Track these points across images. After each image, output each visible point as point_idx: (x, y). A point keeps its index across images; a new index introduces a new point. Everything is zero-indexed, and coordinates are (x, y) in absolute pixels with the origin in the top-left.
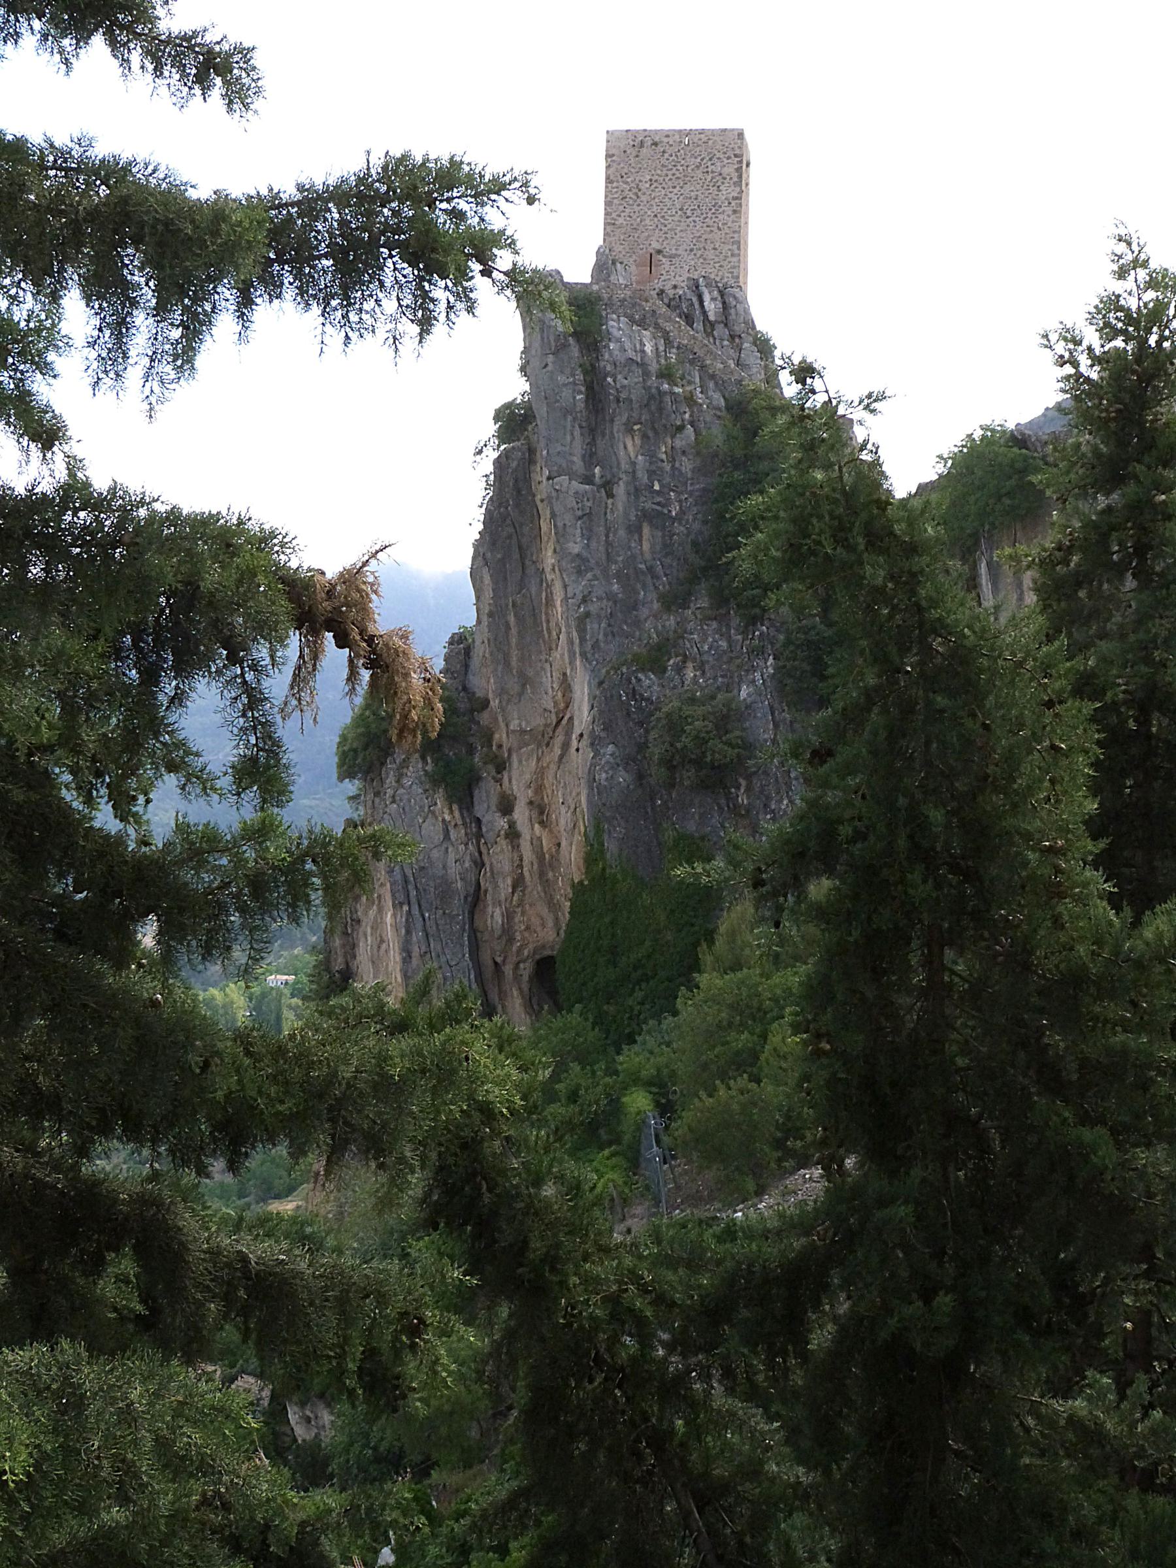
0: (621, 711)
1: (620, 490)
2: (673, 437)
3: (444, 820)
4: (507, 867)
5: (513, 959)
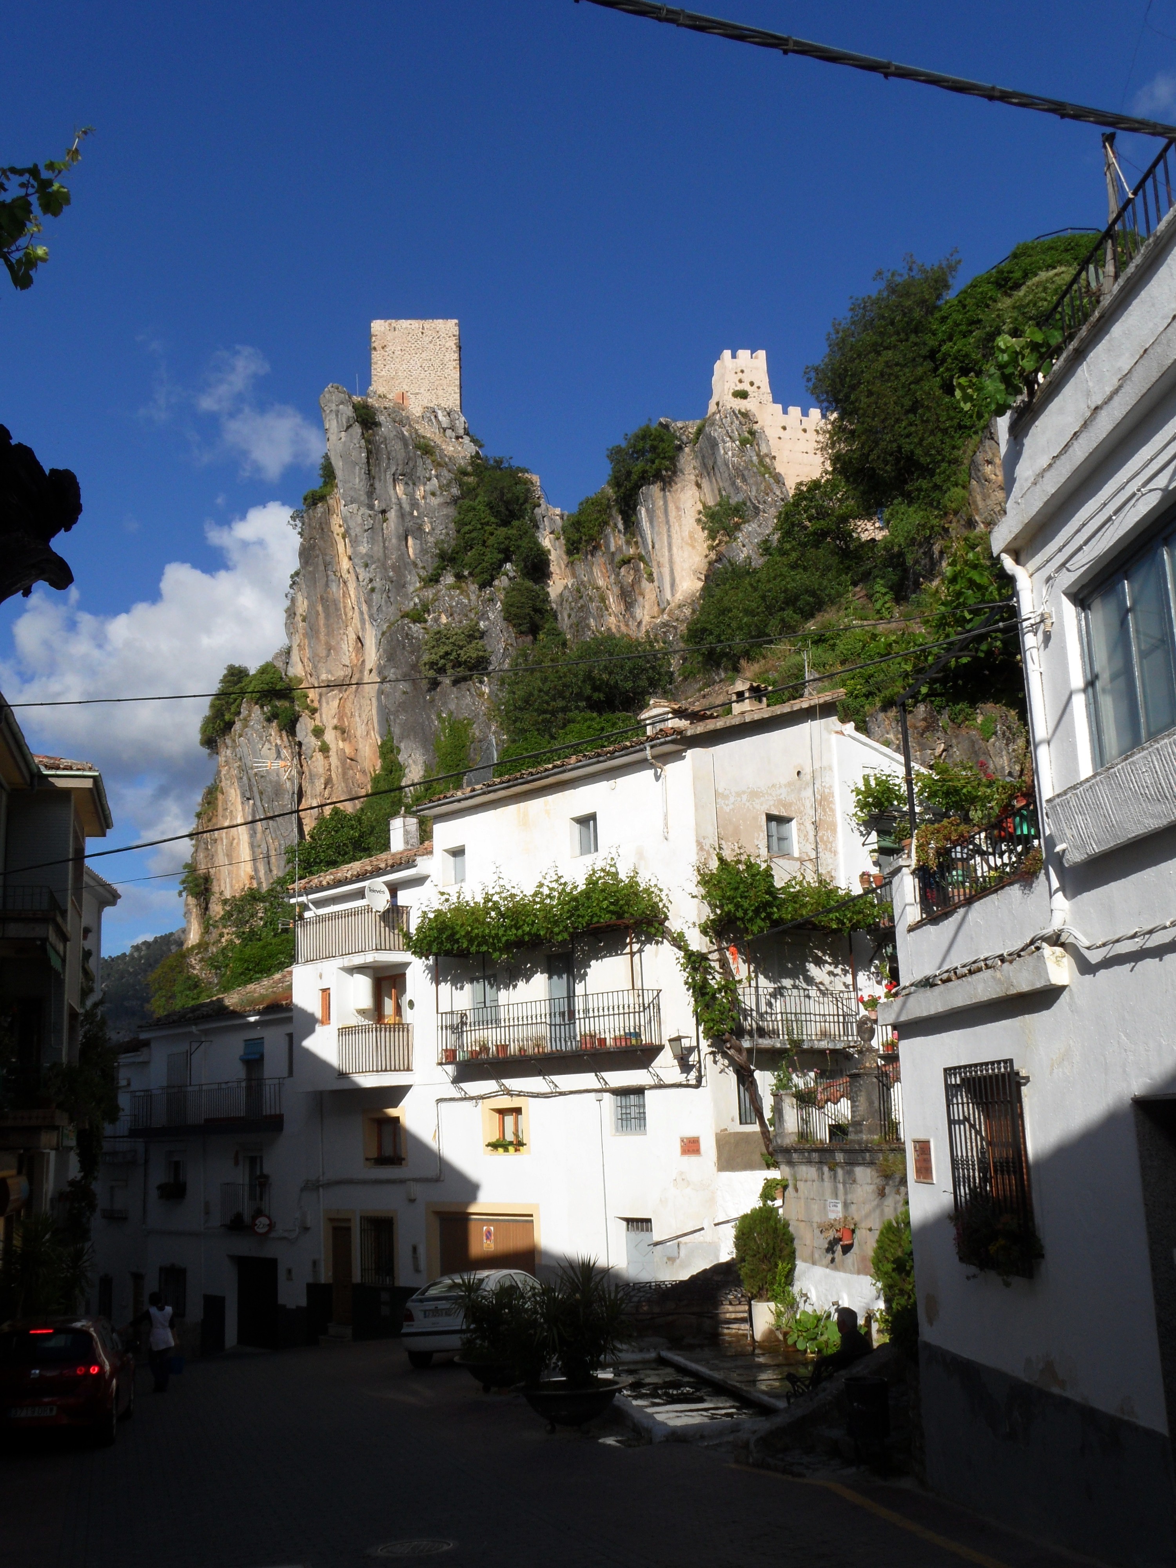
0: (394, 646)
1: (392, 515)
2: (425, 484)
3: (276, 745)
4: (321, 770)
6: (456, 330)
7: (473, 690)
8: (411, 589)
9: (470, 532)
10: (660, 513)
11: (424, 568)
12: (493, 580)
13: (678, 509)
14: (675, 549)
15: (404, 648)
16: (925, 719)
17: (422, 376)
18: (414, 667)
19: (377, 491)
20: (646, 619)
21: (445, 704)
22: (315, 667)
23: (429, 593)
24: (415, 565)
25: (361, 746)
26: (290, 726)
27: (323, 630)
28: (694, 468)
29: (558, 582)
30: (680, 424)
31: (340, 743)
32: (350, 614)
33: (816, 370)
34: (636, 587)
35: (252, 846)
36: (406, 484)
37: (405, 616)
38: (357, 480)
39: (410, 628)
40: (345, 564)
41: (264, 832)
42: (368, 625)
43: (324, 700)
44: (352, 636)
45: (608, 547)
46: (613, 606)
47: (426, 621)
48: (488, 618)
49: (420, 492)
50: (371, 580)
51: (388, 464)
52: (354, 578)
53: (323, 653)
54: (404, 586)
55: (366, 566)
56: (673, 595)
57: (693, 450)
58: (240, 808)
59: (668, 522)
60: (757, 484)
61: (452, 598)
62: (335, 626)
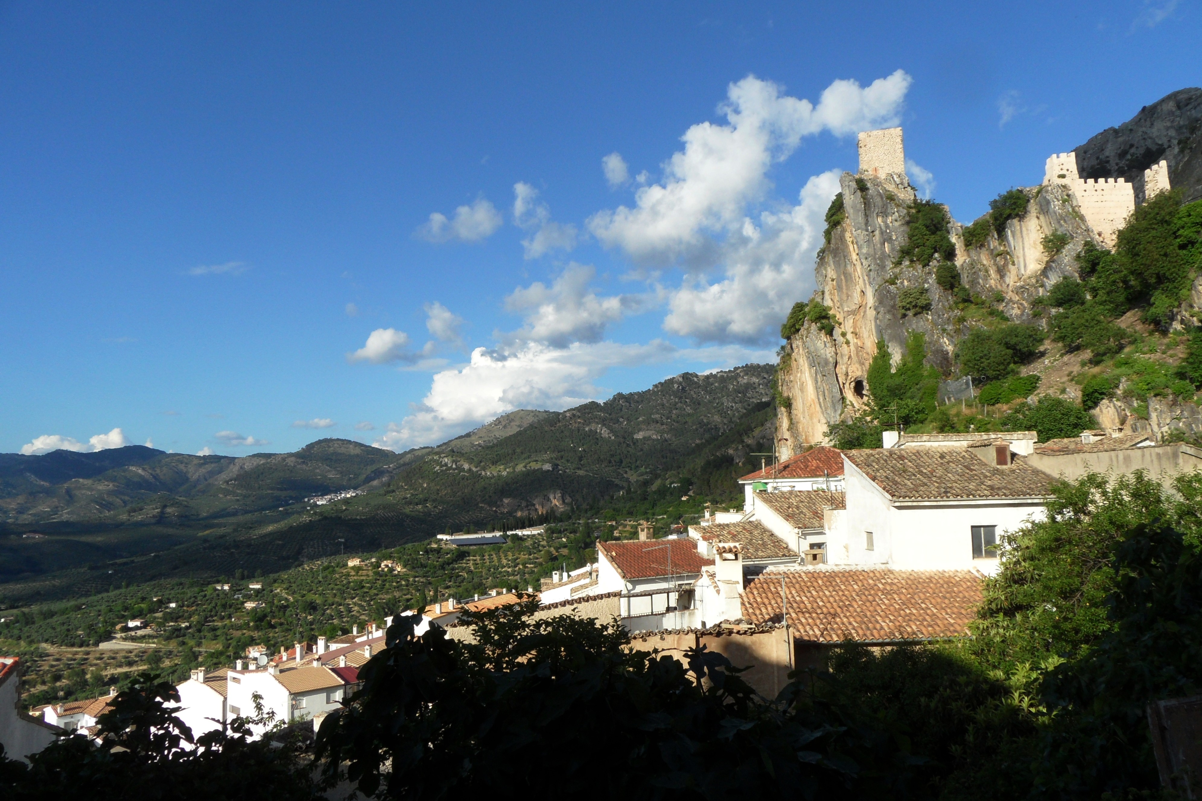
0: (882, 297)
1: (877, 233)
5: (848, 382)
6: (901, 133)
13: (1027, 230)
14: (1026, 250)
18: (893, 306)
20: (1012, 283)
21: (910, 325)
22: (841, 305)
23: (897, 270)
24: (889, 256)
26: (830, 333)
27: (844, 287)
31: (855, 340)
33: (1119, 231)
35: (817, 388)
37: (887, 282)
40: (854, 256)
42: (868, 286)
44: (859, 290)
45: (989, 246)
49: (889, 220)
53: (845, 299)
55: (866, 258)
58: (807, 369)
60: (1072, 224)
61: (909, 272)
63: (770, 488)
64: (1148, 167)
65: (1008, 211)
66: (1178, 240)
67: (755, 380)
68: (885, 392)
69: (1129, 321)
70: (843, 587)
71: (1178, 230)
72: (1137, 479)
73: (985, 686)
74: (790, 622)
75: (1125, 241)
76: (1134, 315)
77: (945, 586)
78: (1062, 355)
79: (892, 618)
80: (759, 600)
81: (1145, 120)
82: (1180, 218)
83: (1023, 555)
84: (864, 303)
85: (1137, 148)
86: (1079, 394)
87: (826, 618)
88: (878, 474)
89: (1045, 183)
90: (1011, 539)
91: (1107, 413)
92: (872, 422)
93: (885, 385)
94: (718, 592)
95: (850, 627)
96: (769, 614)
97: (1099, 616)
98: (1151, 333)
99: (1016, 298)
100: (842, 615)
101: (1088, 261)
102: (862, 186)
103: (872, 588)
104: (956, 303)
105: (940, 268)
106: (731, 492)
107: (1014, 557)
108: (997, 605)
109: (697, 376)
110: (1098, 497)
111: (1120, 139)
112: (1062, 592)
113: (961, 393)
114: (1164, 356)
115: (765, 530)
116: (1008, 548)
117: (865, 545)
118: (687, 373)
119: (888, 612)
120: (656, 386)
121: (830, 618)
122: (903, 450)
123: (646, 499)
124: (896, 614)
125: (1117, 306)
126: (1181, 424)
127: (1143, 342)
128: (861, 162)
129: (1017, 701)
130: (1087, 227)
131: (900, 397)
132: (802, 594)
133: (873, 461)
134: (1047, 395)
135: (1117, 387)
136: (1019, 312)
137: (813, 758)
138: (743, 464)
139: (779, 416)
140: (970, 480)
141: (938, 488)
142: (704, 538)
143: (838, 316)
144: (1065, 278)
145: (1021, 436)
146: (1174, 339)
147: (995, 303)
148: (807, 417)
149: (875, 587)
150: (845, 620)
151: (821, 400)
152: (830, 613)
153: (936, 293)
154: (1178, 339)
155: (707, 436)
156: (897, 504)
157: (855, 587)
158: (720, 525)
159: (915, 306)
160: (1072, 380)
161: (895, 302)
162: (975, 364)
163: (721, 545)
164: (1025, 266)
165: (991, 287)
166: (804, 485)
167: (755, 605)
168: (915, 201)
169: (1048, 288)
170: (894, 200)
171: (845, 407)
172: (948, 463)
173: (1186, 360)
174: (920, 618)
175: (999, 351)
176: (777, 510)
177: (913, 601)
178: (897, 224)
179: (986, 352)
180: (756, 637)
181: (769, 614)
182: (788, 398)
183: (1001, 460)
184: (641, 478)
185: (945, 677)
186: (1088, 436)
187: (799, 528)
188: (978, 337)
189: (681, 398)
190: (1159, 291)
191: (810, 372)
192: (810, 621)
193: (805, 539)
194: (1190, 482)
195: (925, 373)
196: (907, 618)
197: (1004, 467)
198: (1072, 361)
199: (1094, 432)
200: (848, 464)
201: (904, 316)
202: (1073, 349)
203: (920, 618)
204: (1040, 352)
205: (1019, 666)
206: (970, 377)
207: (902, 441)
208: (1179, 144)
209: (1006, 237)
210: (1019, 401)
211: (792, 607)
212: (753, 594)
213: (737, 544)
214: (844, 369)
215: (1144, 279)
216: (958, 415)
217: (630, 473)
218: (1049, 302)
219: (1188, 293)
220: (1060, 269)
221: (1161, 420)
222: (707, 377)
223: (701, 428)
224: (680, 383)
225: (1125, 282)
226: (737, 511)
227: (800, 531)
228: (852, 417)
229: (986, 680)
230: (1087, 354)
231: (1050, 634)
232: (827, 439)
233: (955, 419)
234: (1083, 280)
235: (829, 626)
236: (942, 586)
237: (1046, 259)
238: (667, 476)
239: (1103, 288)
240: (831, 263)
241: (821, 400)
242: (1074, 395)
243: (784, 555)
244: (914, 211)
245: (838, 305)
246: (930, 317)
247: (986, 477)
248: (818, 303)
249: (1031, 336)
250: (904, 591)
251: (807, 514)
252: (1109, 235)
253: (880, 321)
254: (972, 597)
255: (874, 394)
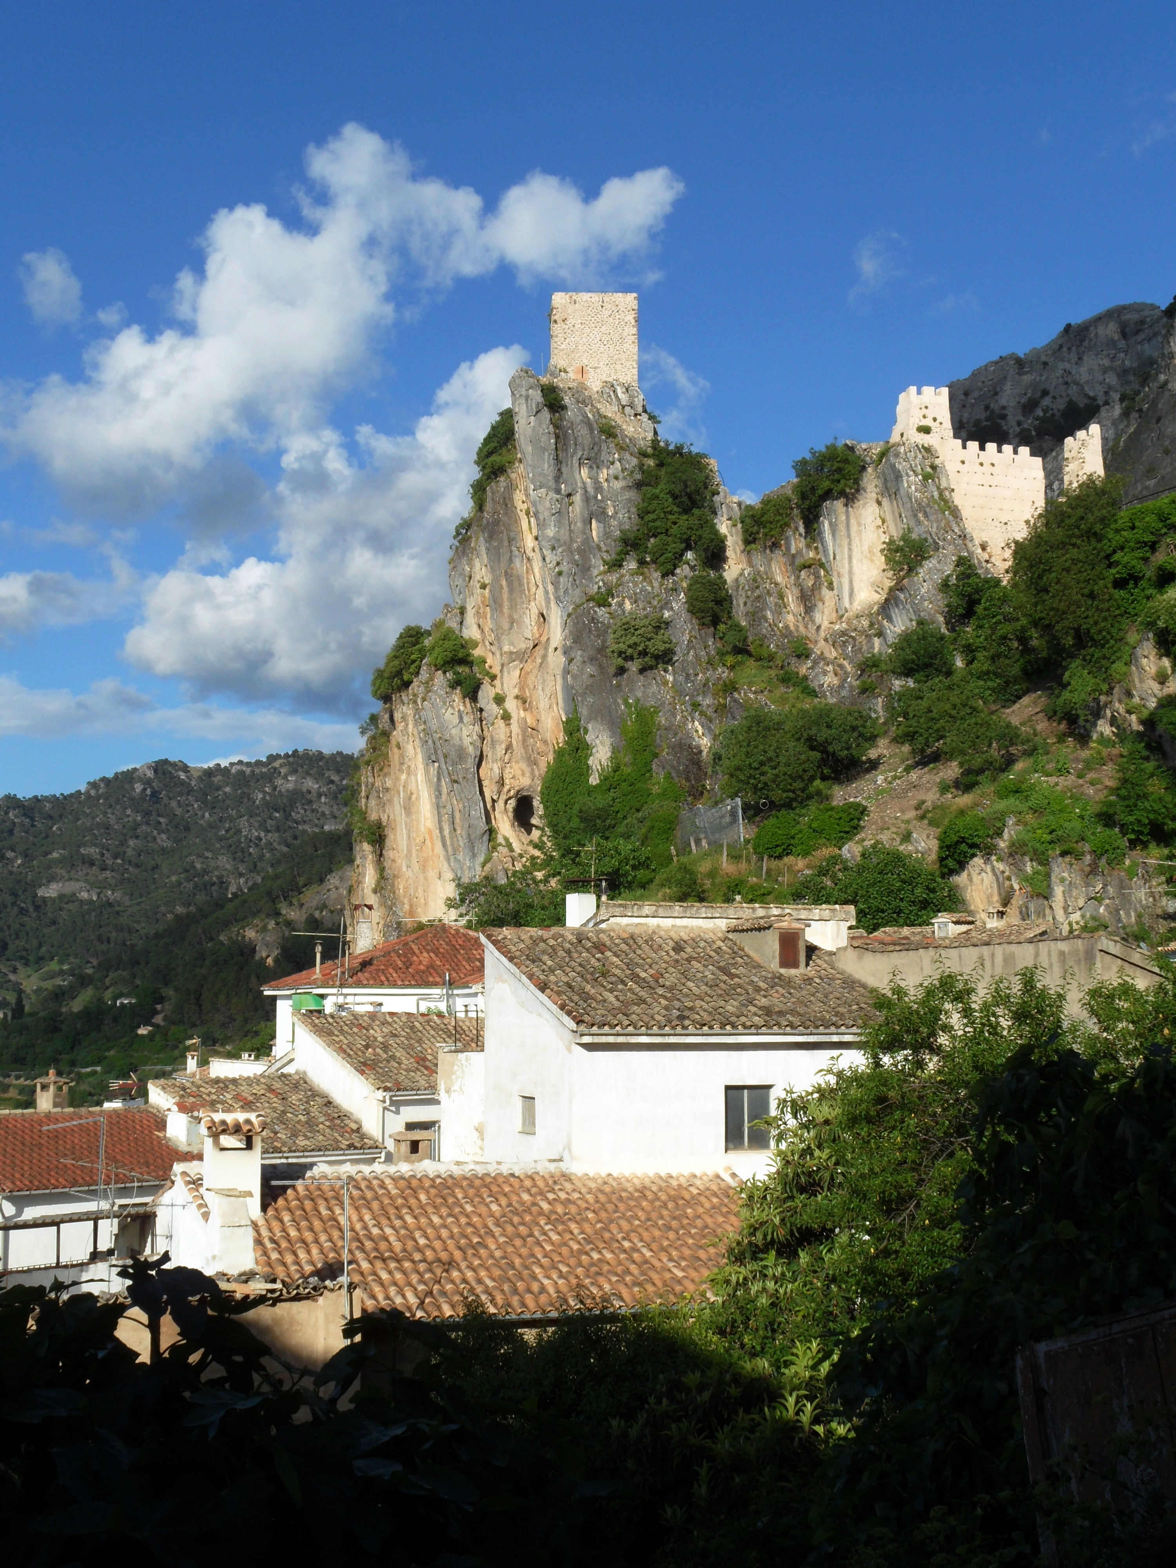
0: (581, 629)
1: (578, 498)
2: (608, 468)
3: (459, 711)
6: (634, 304)
7: (658, 678)
8: (595, 572)
9: (654, 521)
10: (842, 527)
11: (607, 552)
12: (675, 568)
13: (859, 524)
14: (854, 561)
15: (590, 631)
16: (1090, 865)
17: (602, 350)
18: (601, 650)
19: (564, 476)
20: (825, 624)
21: (632, 690)
22: (498, 638)
23: (613, 578)
24: (599, 548)
25: (543, 718)
26: (472, 694)
27: (506, 604)
28: (876, 486)
29: (733, 567)
30: (864, 446)
31: (522, 714)
32: (533, 589)
33: (1016, 542)
34: (816, 593)
35: (438, 807)
36: (591, 467)
38: (546, 466)
39: (595, 612)
40: (529, 542)
41: (448, 794)
42: (553, 604)
43: (505, 669)
44: (535, 611)
45: (788, 548)
46: (792, 605)
47: (610, 605)
48: (672, 608)
49: (603, 475)
50: (558, 564)
51: (575, 449)
52: (540, 558)
53: (506, 626)
54: (589, 569)
55: (553, 548)
56: (851, 604)
57: (875, 469)
58: (421, 766)
59: (849, 536)
60: (938, 522)
61: (636, 584)
62: (518, 600)
63: (329, 1007)
64: (1072, 433)
65: (826, 484)
66: (1113, 571)
67: (311, 784)
68: (575, 823)
69: (1026, 712)
70: (469, 1208)
71: (1114, 552)
72: (1025, 986)
73: (734, 1391)
74: (357, 1278)
75: (1026, 563)
76: (1035, 703)
77: (671, 1205)
78: (908, 770)
79: (564, 1269)
80: (293, 1233)
81: (1069, 349)
82: (1117, 531)
83: (818, 1137)
84: (544, 639)
85: (1054, 398)
86: (934, 844)
87: (430, 1271)
88: (552, 978)
89: (895, 438)
90: (797, 1106)
91: (979, 882)
92: (546, 881)
93: (577, 807)
94: (206, 1216)
95: (479, 1289)
96: (312, 1263)
97: (944, 1244)
98: (1061, 739)
99: (832, 653)
100: (463, 1265)
101: (962, 595)
102: (553, 401)
103: (528, 1211)
104: (722, 654)
105: (695, 581)
106: (246, 1020)
107: (802, 1142)
108: (765, 1236)
109: (185, 768)
110: (956, 1020)
111: (1027, 378)
112: (883, 1201)
113: (720, 828)
114: (1081, 781)
115: (314, 1094)
116: (792, 1123)
117: (518, 1123)
118: (166, 762)
119: (557, 1258)
120: (93, 785)
121: (438, 1271)
122: (603, 931)
123: (56, 1029)
124: (572, 1261)
125: (1007, 683)
126: (1102, 910)
127: (1047, 753)
128: (554, 352)
129: (791, 1411)
130: (963, 530)
131: (604, 828)
132: (384, 1222)
133: (544, 952)
134: (877, 842)
135: (999, 834)
136: (836, 681)
137: (385, 1470)
138: (276, 960)
139: (358, 861)
140: (727, 995)
141: (666, 1008)
142: (183, 1108)
143: (489, 661)
144: (921, 623)
145: (826, 914)
146: (1099, 753)
147: (793, 660)
148: (416, 867)
149: (534, 1209)
150: (469, 1274)
151: (447, 832)
152: (439, 1260)
153: (684, 631)
154: (1105, 752)
155: (201, 898)
156: (587, 1040)
157: (494, 1207)
158: (217, 1081)
159: (644, 653)
160: (922, 817)
161: (604, 641)
162: (751, 777)
163: (218, 1117)
164: (851, 594)
165: (787, 627)
166: (401, 1001)
167: (284, 1244)
168: (655, 443)
169: (890, 640)
170: (614, 436)
171: (494, 848)
172: (689, 960)
173: (1114, 791)
174: (619, 1270)
175: (794, 754)
176: (341, 1050)
177: (607, 1235)
178: (617, 485)
179: (771, 754)
180: (282, 1309)
181: (312, 1263)
182: (379, 825)
183: (788, 958)
184: (48, 985)
185: (661, 1376)
186: (946, 924)
187: (386, 1089)
188: (758, 723)
189: (148, 814)
190: (1078, 661)
191: (427, 772)
192: (398, 1276)
193: (397, 1112)
194: (1111, 997)
195: (656, 790)
196: (593, 1269)
197: (793, 972)
198: (924, 780)
199: (956, 916)
200: (492, 957)
201: (621, 671)
202: (927, 759)
203: (619, 1270)
204: (870, 761)
205: (799, 1348)
206: (738, 800)
207: (603, 914)
208: (1122, 400)
209: (820, 533)
210: (826, 852)
211: (362, 1249)
212: (281, 1221)
213: (252, 1116)
214: (496, 771)
215: (1054, 637)
216: (712, 874)
217: (22, 971)
218: (890, 667)
219: (1124, 669)
220: (913, 604)
221: (1070, 898)
222: (208, 773)
223: (189, 880)
224: (148, 782)
225: (1023, 640)
226: (257, 1058)
227: (388, 1095)
228: (506, 871)
229: (737, 1379)
230: (952, 770)
231: (858, 1283)
232: (453, 914)
233: (708, 883)
234: (952, 630)
235: (436, 1287)
236: (665, 1205)
237: (888, 584)
238: (107, 981)
239: (985, 648)
240: (483, 552)
241: (447, 832)
242: (924, 845)
243: (351, 1146)
244: (651, 462)
245: (491, 637)
246: (670, 678)
247: (758, 990)
248: (450, 631)
249: (854, 728)
250: (590, 1215)
251: (403, 1062)
252: (1000, 551)
253: (574, 677)
254: (720, 1226)
255: (553, 826)
